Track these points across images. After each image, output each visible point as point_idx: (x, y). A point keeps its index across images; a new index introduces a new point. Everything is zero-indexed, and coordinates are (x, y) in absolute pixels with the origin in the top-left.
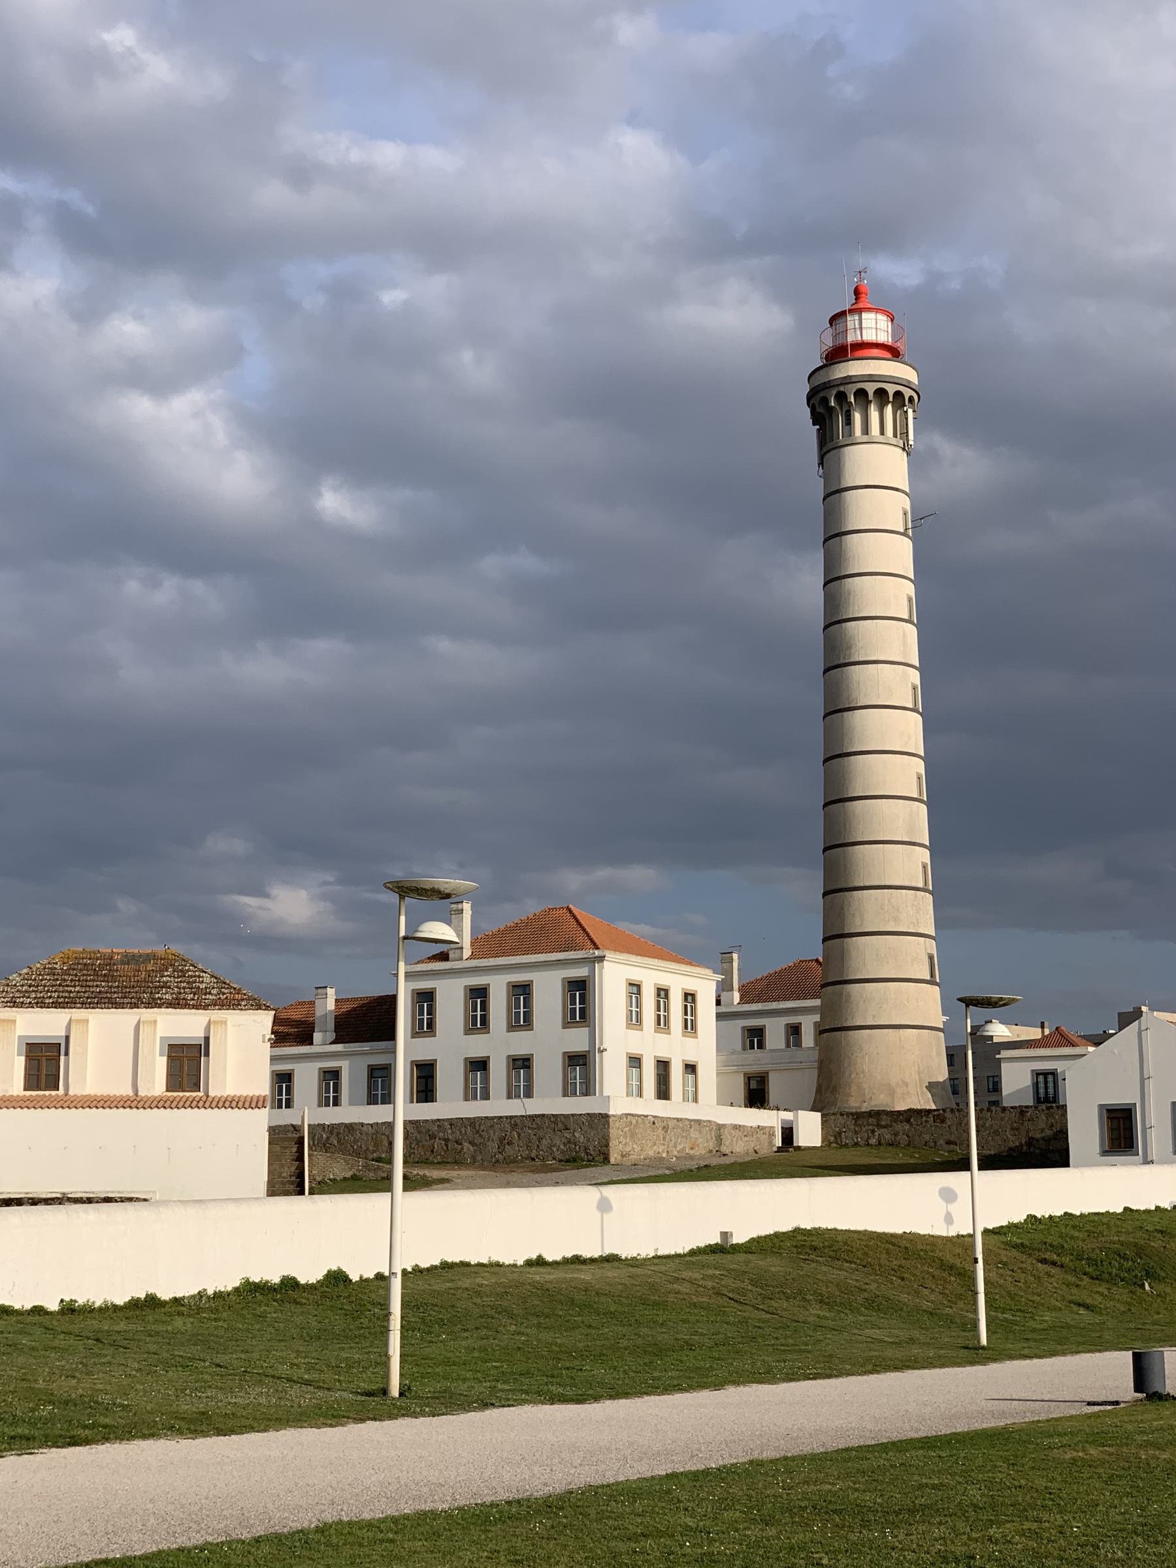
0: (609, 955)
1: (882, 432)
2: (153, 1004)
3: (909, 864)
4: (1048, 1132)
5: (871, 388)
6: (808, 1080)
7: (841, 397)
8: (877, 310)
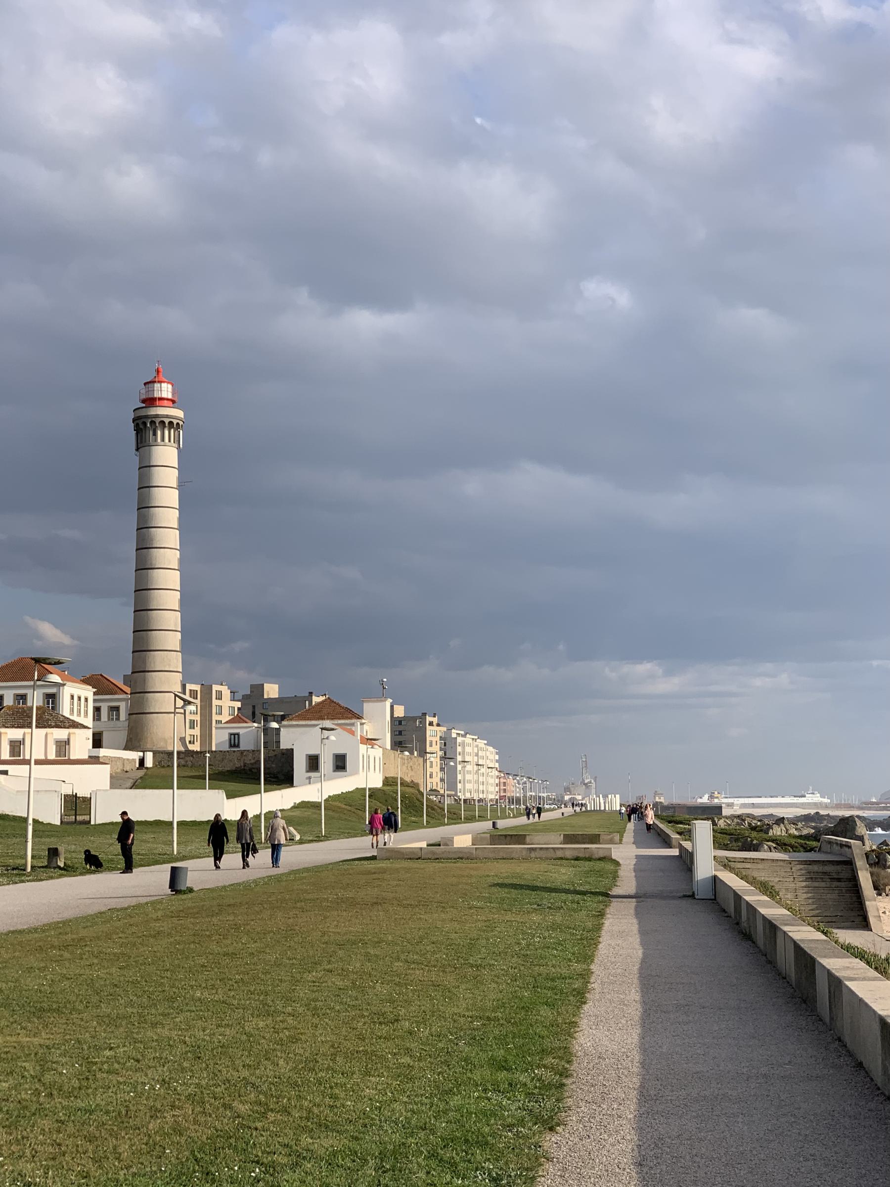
0: (68, 683)
1: (170, 441)
2: (50, 727)
3: (173, 640)
4: (253, 761)
5: (167, 421)
6: (123, 736)
7: (153, 423)
8: (168, 383)
